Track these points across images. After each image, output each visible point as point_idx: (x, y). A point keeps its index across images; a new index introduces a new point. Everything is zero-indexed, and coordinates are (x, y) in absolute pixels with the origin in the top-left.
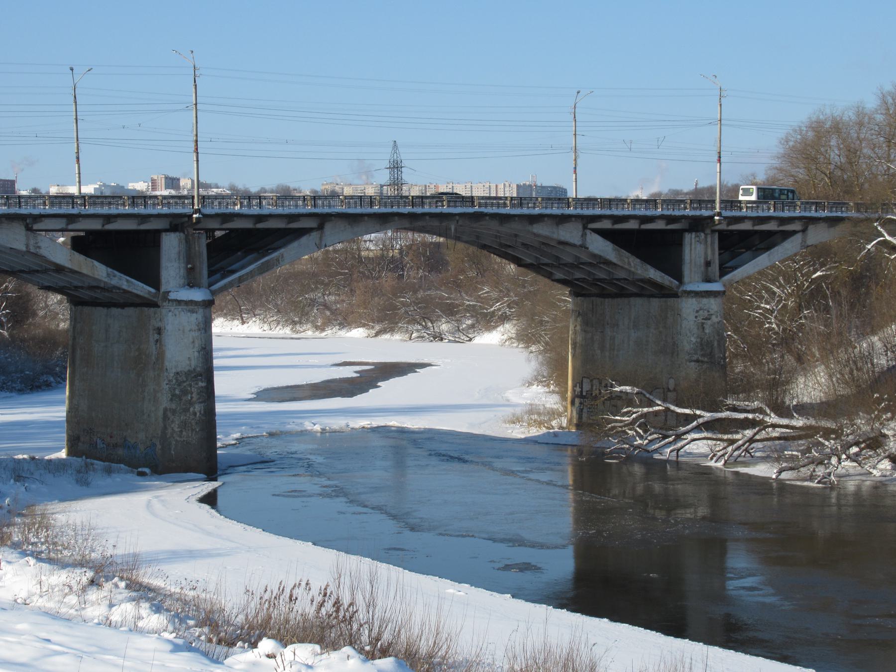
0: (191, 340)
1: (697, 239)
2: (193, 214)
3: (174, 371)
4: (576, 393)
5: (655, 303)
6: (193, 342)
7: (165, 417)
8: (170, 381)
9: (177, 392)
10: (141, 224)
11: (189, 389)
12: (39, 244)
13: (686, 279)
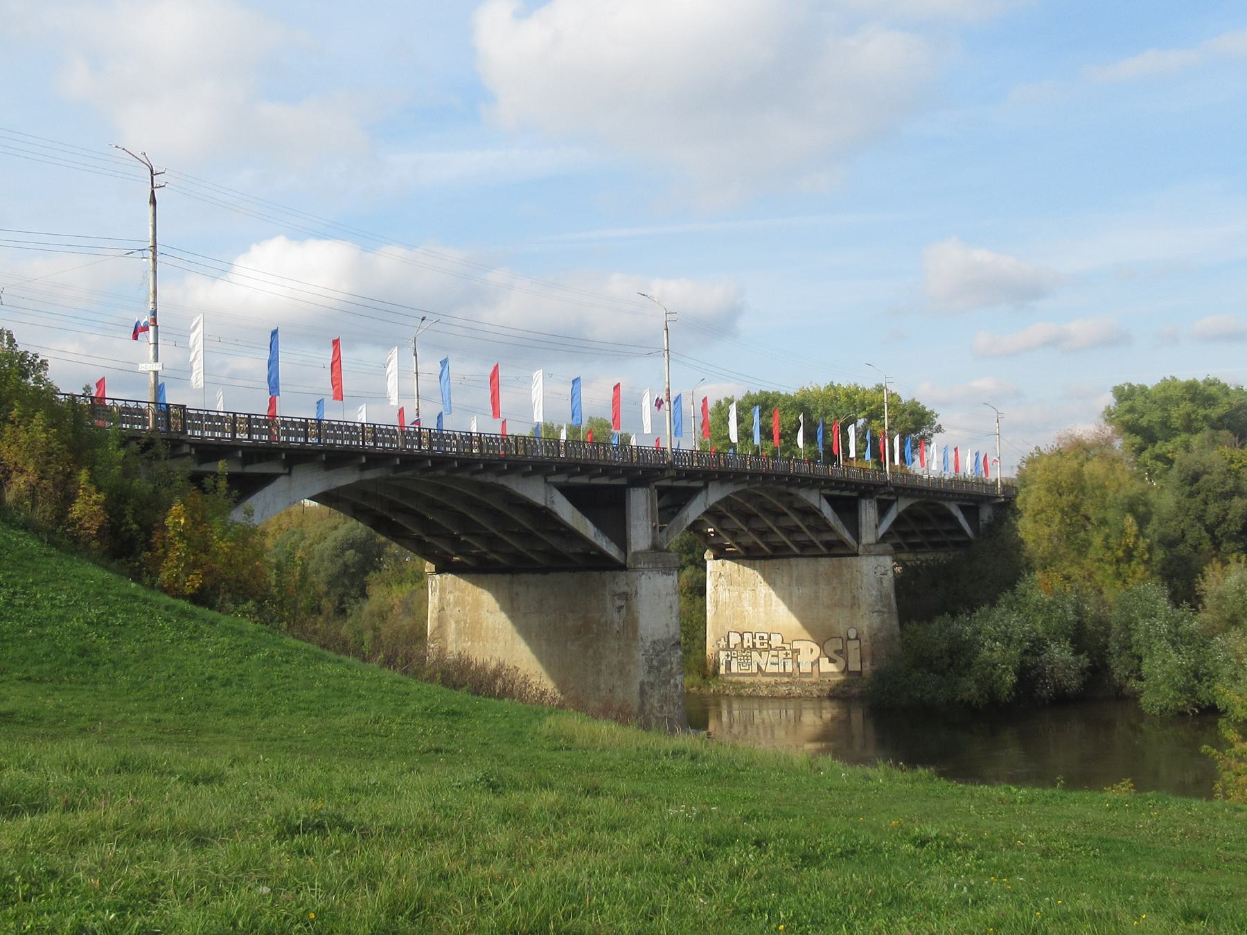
0: (668, 604)
3: (650, 639)
5: (824, 564)
6: (671, 607)
7: (642, 692)
8: (646, 651)
9: (655, 663)
10: (202, 463)
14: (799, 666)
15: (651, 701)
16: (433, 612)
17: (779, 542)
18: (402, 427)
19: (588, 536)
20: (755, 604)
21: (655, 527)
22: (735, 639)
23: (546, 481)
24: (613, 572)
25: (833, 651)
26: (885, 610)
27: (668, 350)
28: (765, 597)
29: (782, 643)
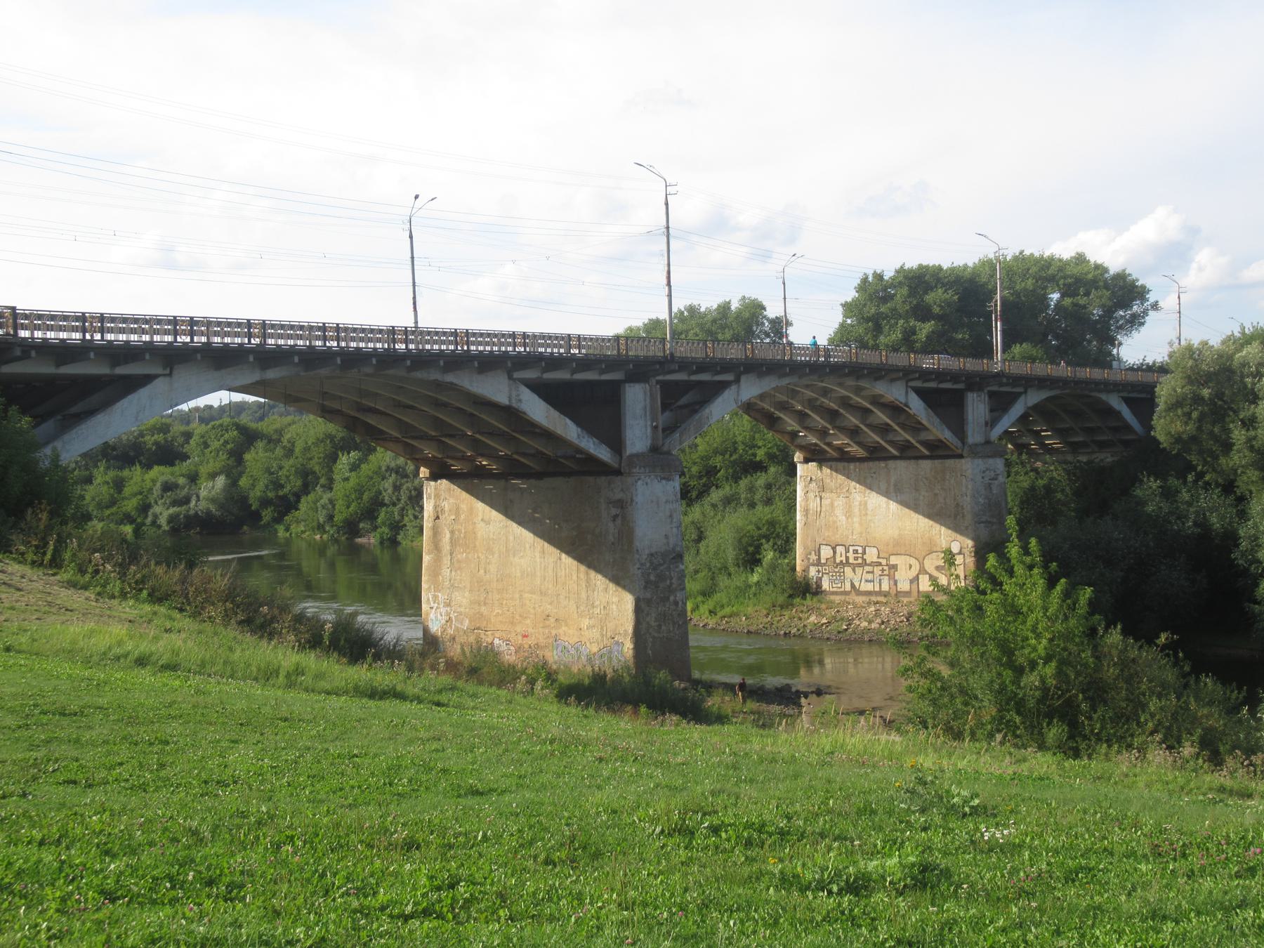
1: (979, 399)
3: (647, 552)
6: (671, 516)
8: (642, 564)
9: (652, 578)
12: (521, 397)
14: (896, 584)
15: (648, 619)
16: (428, 521)
17: (872, 443)
18: (416, 327)
19: (569, 438)
20: (849, 514)
21: (656, 427)
22: (826, 552)
23: (510, 377)
24: (609, 477)
26: (995, 520)
29: (878, 557)
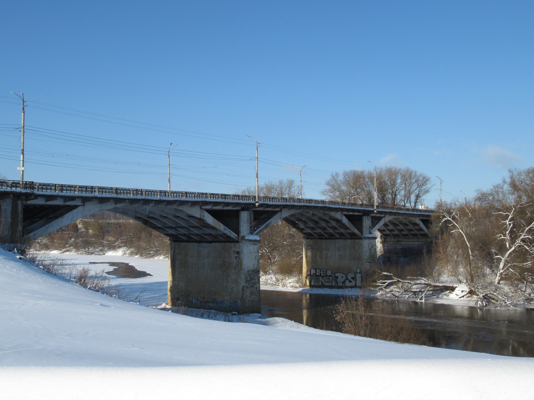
2: (256, 203)
3: (247, 270)
4: (308, 274)
5: (349, 242)
6: (256, 257)
7: (243, 290)
9: (248, 279)
10: (213, 207)
11: (254, 277)
13: (364, 233)
15: (247, 293)
19: (221, 229)
23: (201, 208)
24: (235, 243)
25: (350, 278)
27: (258, 158)
28: (325, 254)
29: (331, 274)
